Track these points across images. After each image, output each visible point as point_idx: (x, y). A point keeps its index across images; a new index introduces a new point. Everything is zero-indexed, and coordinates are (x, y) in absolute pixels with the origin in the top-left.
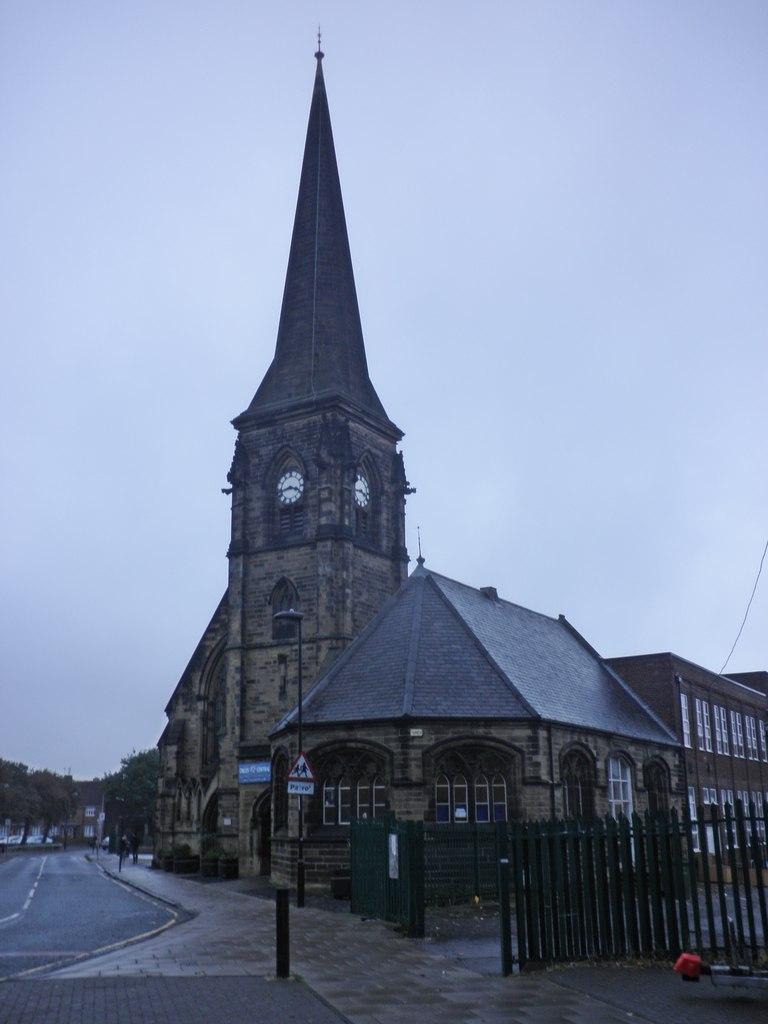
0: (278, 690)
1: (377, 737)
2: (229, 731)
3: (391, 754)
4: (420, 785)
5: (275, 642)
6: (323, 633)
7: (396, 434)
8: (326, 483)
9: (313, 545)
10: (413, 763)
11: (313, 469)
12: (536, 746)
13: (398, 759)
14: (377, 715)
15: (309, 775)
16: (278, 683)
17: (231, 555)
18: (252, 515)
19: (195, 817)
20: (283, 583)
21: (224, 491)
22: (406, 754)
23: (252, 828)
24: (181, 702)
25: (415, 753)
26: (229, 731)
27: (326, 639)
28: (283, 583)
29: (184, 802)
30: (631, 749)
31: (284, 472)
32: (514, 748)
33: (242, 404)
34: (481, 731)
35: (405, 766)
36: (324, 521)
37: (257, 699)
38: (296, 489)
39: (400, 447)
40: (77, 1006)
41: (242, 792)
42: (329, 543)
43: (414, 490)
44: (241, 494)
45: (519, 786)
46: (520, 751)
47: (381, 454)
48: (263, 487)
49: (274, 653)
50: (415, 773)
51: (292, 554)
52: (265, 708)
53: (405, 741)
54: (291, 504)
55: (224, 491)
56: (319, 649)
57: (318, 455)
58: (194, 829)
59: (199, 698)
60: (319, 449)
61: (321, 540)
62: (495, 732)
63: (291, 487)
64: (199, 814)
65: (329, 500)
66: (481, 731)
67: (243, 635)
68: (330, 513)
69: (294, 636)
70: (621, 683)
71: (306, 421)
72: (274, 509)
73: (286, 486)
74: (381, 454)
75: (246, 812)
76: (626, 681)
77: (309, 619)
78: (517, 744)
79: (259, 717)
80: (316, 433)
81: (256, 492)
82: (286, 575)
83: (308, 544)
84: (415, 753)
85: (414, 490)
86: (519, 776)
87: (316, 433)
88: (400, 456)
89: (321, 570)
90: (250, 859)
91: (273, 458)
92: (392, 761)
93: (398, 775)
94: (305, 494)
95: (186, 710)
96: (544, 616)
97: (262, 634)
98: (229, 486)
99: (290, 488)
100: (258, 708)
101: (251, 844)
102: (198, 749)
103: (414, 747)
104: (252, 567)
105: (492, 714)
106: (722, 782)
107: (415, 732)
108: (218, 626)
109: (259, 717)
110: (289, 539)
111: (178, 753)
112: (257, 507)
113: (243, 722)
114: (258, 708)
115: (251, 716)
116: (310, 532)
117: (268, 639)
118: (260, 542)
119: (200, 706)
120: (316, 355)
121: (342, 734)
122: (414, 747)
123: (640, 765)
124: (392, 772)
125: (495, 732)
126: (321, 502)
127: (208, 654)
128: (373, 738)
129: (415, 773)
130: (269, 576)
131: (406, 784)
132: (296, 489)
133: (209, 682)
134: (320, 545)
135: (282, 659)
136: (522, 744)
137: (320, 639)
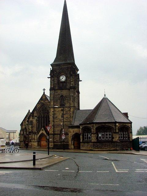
0: (61, 116)
1: (111, 125)
2: (51, 123)
4: (118, 133)
8: (72, 78)
9: (69, 90)
11: (69, 75)
13: (115, 129)
16: (61, 114)
17: (50, 90)
19: (36, 139)
20: (62, 96)
22: (116, 128)
23: (72, 141)
25: (117, 128)
26: (51, 123)
27: (72, 107)
28: (62, 96)
29: (33, 136)
31: (61, 75)
32: (129, 127)
33: (52, 61)
34: (125, 124)
35: (116, 130)
36: (71, 85)
37: (56, 117)
42: (73, 89)
44: (53, 79)
48: (57, 78)
50: (117, 131)
51: (64, 91)
53: (116, 126)
56: (71, 109)
58: (36, 141)
59: (36, 116)
62: (127, 124)
63: (63, 78)
64: (37, 138)
65: (72, 81)
66: (125, 124)
71: (67, 66)
79: (57, 121)
80: (65, 71)
81: (56, 78)
82: (63, 95)
84: (117, 128)
87: (65, 71)
89: (71, 95)
92: (113, 129)
96: (37, 105)
98: (50, 76)
100: (57, 119)
101: (72, 143)
102: (35, 126)
104: (55, 93)
107: (117, 124)
108: (40, 103)
109: (57, 121)
111: (31, 127)
112: (56, 82)
113: (54, 121)
114: (57, 119)
115: (55, 120)
116: (68, 87)
118: (57, 88)
119: (36, 118)
121: (104, 124)
125: (127, 124)
126: (71, 82)
128: (110, 125)
131: (116, 133)
133: (37, 114)
134: (71, 90)
137: (71, 107)
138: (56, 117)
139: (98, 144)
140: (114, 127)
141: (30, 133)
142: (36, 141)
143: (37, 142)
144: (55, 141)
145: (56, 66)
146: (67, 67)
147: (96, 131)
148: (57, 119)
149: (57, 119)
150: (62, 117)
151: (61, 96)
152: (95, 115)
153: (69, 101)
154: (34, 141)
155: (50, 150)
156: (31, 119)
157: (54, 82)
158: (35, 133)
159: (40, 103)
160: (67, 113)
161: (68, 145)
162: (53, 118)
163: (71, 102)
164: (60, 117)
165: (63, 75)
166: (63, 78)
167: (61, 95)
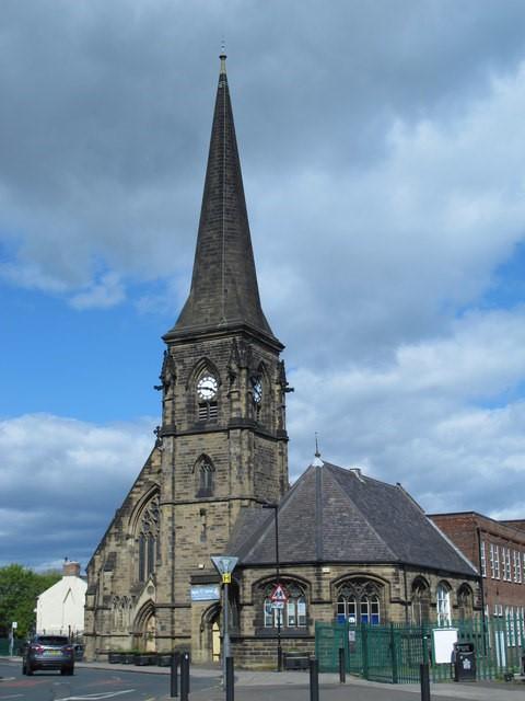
2: (164, 563)
3: (310, 583)
5: (197, 500)
6: (234, 495)
7: (277, 347)
9: (227, 431)
10: (324, 589)
12: (397, 579)
14: (301, 558)
15: (284, 598)
18: (178, 407)
21: (156, 387)
24: (113, 538)
25: (325, 583)
26: (164, 563)
28: (204, 457)
30: (449, 580)
32: (384, 580)
34: (364, 569)
35: (319, 591)
36: (234, 415)
37: (184, 540)
38: (211, 390)
39: (282, 357)
40: (493, 673)
41: (194, 606)
43: (292, 390)
45: (388, 603)
46: (388, 582)
47: (269, 363)
49: (197, 508)
52: (191, 547)
54: (207, 400)
55: (156, 387)
57: (230, 368)
60: (230, 362)
61: (233, 429)
62: (373, 570)
65: (238, 400)
66: (364, 569)
67: (173, 494)
68: (239, 409)
69: (212, 496)
70: (440, 532)
72: (194, 404)
73: (205, 385)
74: (269, 363)
75: (196, 620)
76: (443, 530)
77: (221, 485)
78: (385, 577)
79: (185, 553)
82: (205, 452)
83: (223, 431)
84: (325, 583)
85: (292, 390)
86: (388, 598)
88: (283, 363)
89: (232, 450)
90: (199, 651)
91: (194, 367)
93: (315, 596)
94: (219, 394)
95: (118, 545)
97: (187, 494)
98: (160, 383)
99: (207, 388)
103: (325, 579)
105: (372, 559)
106: (506, 601)
108: (142, 483)
109: (185, 553)
110: (207, 426)
111: (112, 577)
115: (178, 552)
116: (224, 422)
117: (192, 497)
120: (226, 291)
122: (325, 579)
123: (455, 590)
124: (311, 595)
125: (373, 570)
127: (135, 504)
129: (326, 595)
130: (193, 452)
131: (320, 602)
132: (211, 390)
135: (203, 513)
136: (389, 578)
138: (184, 540)
139: (260, 644)
140: (313, 579)
141: (106, 599)
142: (126, 633)
143: (130, 639)
144: (178, 631)
145: (184, 342)
146: (221, 345)
147: (252, 596)
148: (187, 546)
149: (187, 546)
150: (204, 537)
151: (199, 460)
152: (406, 502)
153: (227, 476)
154: (119, 633)
155: (399, 674)
156: (112, 546)
157: (174, 403)
158: (124, 603)
159: (142, 483)
160: (220, 522)
161: (189, 647)
162: (173, 543)
163: (234, 480)
164: (196, 540)
165: (207, 376)
166: (207, 387)
167: (198, 454)
